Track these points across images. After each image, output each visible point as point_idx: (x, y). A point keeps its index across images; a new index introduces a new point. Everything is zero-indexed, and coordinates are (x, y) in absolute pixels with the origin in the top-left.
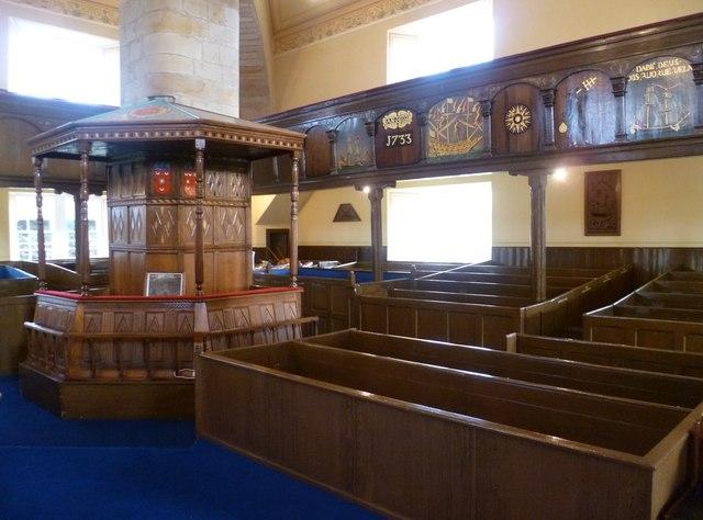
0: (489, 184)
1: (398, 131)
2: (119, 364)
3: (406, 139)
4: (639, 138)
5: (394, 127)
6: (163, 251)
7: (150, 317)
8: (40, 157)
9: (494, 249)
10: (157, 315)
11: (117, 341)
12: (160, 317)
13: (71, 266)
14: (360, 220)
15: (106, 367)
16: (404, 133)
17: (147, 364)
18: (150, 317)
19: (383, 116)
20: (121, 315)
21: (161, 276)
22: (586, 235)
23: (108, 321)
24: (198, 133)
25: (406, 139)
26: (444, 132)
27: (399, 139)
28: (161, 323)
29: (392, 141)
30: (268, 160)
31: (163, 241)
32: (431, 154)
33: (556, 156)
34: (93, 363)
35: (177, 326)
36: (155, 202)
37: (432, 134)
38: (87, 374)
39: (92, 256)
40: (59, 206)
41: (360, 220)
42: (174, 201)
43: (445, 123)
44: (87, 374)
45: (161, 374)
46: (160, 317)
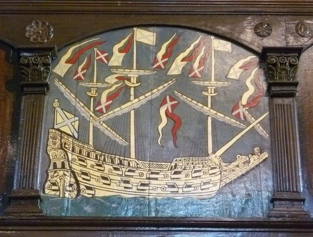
4: (69, 213)
37: (65, 122)
43: (120, 96)
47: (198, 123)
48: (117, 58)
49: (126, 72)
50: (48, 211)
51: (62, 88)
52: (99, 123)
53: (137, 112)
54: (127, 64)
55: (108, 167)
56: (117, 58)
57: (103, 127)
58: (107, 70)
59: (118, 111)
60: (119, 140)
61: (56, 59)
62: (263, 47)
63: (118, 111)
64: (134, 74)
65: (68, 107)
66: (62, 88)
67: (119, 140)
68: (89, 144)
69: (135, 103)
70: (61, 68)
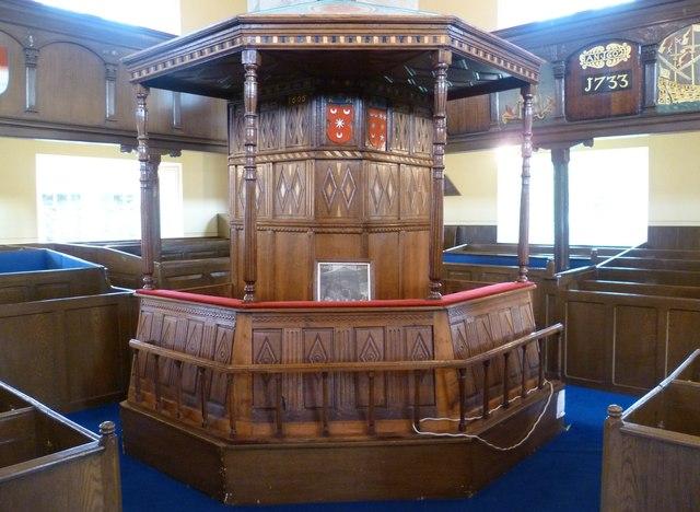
0: (645, 150)
1: (605, 71)
2: (318, 415)
3: (619, 81)
4: (668, 110)
5: (600, 65)
6: (340, 229)
7: (362, 334)
8: (148, 84)
9: (651, 230)
10: (321, 333)
11: (309, 377)
12: (378, 335)
13: (132, 248)
14: (457, 193)
15: (293, 418)
16: (617, 73)
17: (368, 414)
18: (362, 334)
19: (580, 51)
20: (315, 333)
21: (336, 267)
22: (496, 227)
23: (293, 342)
24: (443, 40)
25: (619, 81)
26: (687, 71)
27: (606, 83)
28: (380, 345)
29: (594, 84)
30: (484, 97)
31: (339, 215)
32: (663, 101)
33: (501, 135)
34: (275, 412)
35: (406, 348)
36: (329, 154)
37: (665, 73)
38: (264, 430)
39: (164, 235)
40: (119, 169)
41: (457, 193)
42: (359, 155)
43: (687, 58)
44: (264, 430)
45: (383, 427)
46: (378, 335)
47: (610, 103)
48: (685, 41)
49: (689, 47)
50: (659, 111)
51: (663, 59)
52: (678, 72)
53: (695, 64)
54: (690, 43)
55: (683, 90)
56: (685, 41)
57: (681, 73)
58: (680, 47)
59: (686, 65)
60: (686, 77)
61: (658, 46)
62: (496, 227)
63: (686, 65)
64: (693, 47)
65: (665, 66)
66: (663, 59)
67: (686, 77)
68: (273, 163)
69: (694, 60)
70: (661, 50)
